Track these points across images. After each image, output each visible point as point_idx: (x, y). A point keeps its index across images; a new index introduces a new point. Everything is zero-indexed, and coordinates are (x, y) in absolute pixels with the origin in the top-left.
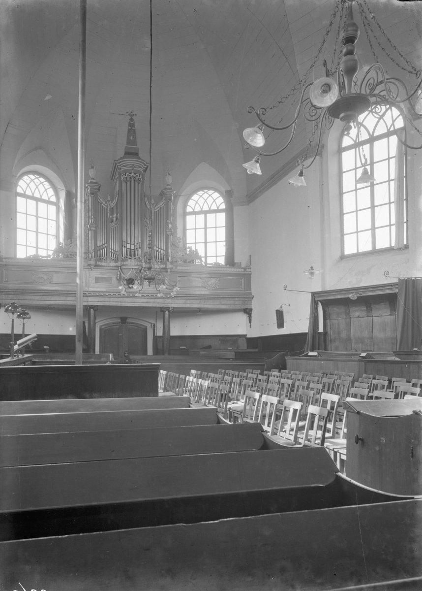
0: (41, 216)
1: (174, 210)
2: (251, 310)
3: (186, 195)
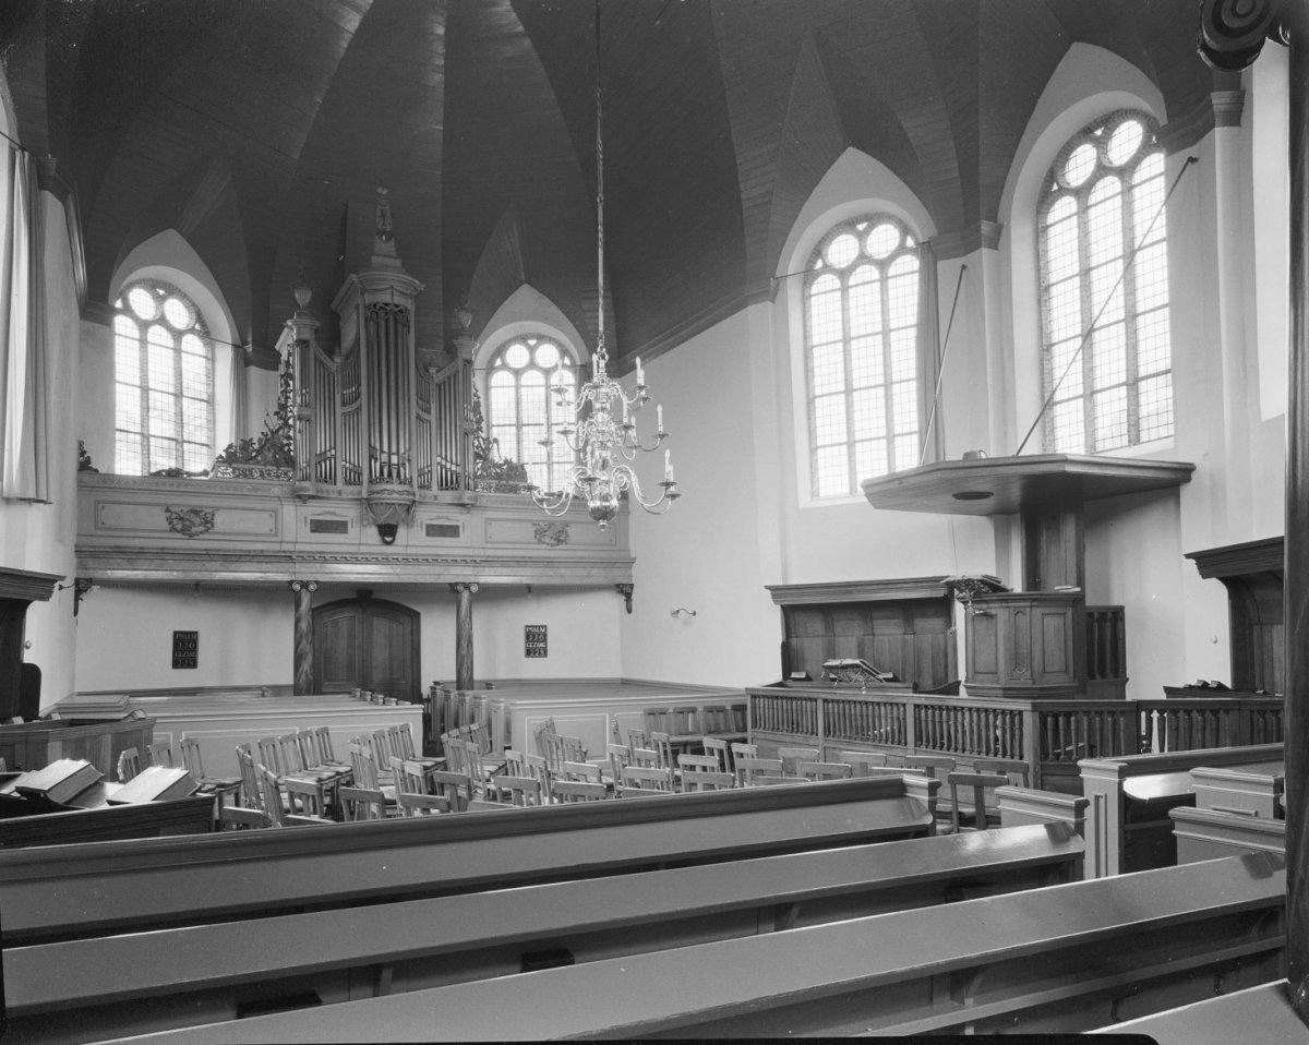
0: (190, 350)
2: (632, 586)
3: (393, 295)
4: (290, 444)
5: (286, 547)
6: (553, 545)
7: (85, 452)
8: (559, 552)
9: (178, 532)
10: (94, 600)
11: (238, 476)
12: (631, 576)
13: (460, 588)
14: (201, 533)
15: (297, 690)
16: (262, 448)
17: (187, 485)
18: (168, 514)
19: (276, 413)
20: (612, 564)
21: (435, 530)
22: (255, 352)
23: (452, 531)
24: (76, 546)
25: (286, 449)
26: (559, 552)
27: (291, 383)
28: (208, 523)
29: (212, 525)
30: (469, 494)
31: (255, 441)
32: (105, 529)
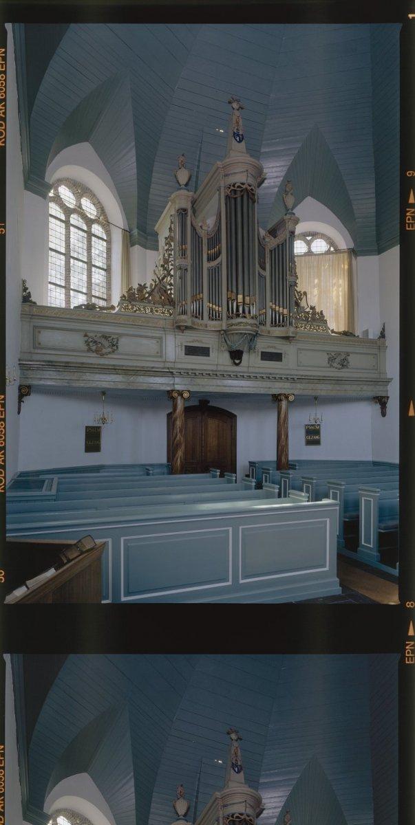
4: (171, 289)
5: (168, 365)
6: (339, 369)
7: (27, 289)
8: (344, 374)
9: (93, 352)
10: (32, 401)
11: (110, 337)
12: (387, 391)
13: (283, 397)
14: (110, 353)
15: (171, 469)
16: (153, 291)
17: (100, 317)
18: (86, 338)
19: (162, 266)
20: (376, 382)
21: (267, 356)
22: (140, 233)
23: (277, 357)
24: (19, 360)
25: (169, 292)
26: (344, 374)
27: (172, 244)
28: (114, 346)
29: (117, 347)
30: (292, 329)
31: (148, 285)
32: (42, 349)
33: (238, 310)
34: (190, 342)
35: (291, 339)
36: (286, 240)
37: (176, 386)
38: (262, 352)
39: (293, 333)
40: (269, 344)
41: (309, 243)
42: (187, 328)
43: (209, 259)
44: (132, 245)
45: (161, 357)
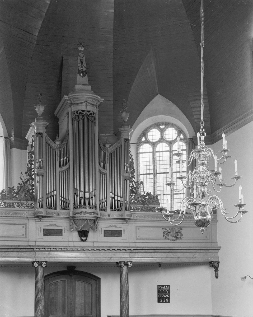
1: (10, 136)
2: (218, 263)
5: (31, 244)
6: (174, 240)
8: (177, 244)
12: (218, 257)
16: (19, 191)
19: (26, 173)
20: (206, 250)
21: (108, 233)
23: (118, 233)
25: (31, 191)
26: (177, 244)
27: (33, 156)
30: (127, 213)
33: (80, 203)
34: (47, 226)
35: (127, 220)
36: (121, 145)
37: (37, 258)
38: (105, 231)
39: (127, 215)
40: (111, 224)
41: (162, 131)
42: (44, 217)
43: (60, 166)
44: (11, 147)
45: (26, 237)
